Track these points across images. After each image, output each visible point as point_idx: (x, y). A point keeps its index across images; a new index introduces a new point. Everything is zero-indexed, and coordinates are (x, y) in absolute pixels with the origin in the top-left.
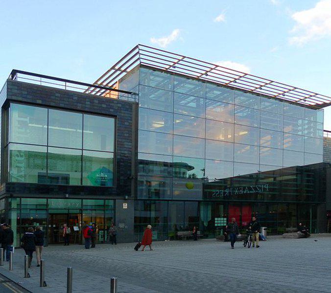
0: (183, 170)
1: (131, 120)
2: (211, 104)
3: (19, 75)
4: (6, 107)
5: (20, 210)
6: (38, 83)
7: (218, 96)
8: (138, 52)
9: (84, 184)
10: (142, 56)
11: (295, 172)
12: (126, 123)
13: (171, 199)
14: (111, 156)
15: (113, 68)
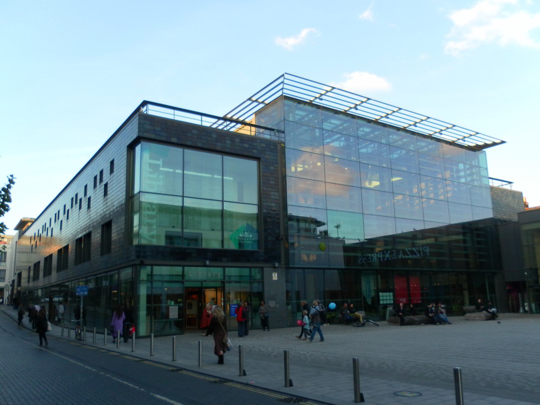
0: (313, 226)
1: (277, 163)
2: (329, 137)
3: (150, 106)
4: (131, 147)
5: (152, 282)
6: (171, 117)
7: (367, 134)
8: (282, 82)
9: (226, 247)
10: (285, 86)
11: (461, 230)
12: (272, 168)
13: (328, 267)
14: (254, 210)
15: (250, 99)
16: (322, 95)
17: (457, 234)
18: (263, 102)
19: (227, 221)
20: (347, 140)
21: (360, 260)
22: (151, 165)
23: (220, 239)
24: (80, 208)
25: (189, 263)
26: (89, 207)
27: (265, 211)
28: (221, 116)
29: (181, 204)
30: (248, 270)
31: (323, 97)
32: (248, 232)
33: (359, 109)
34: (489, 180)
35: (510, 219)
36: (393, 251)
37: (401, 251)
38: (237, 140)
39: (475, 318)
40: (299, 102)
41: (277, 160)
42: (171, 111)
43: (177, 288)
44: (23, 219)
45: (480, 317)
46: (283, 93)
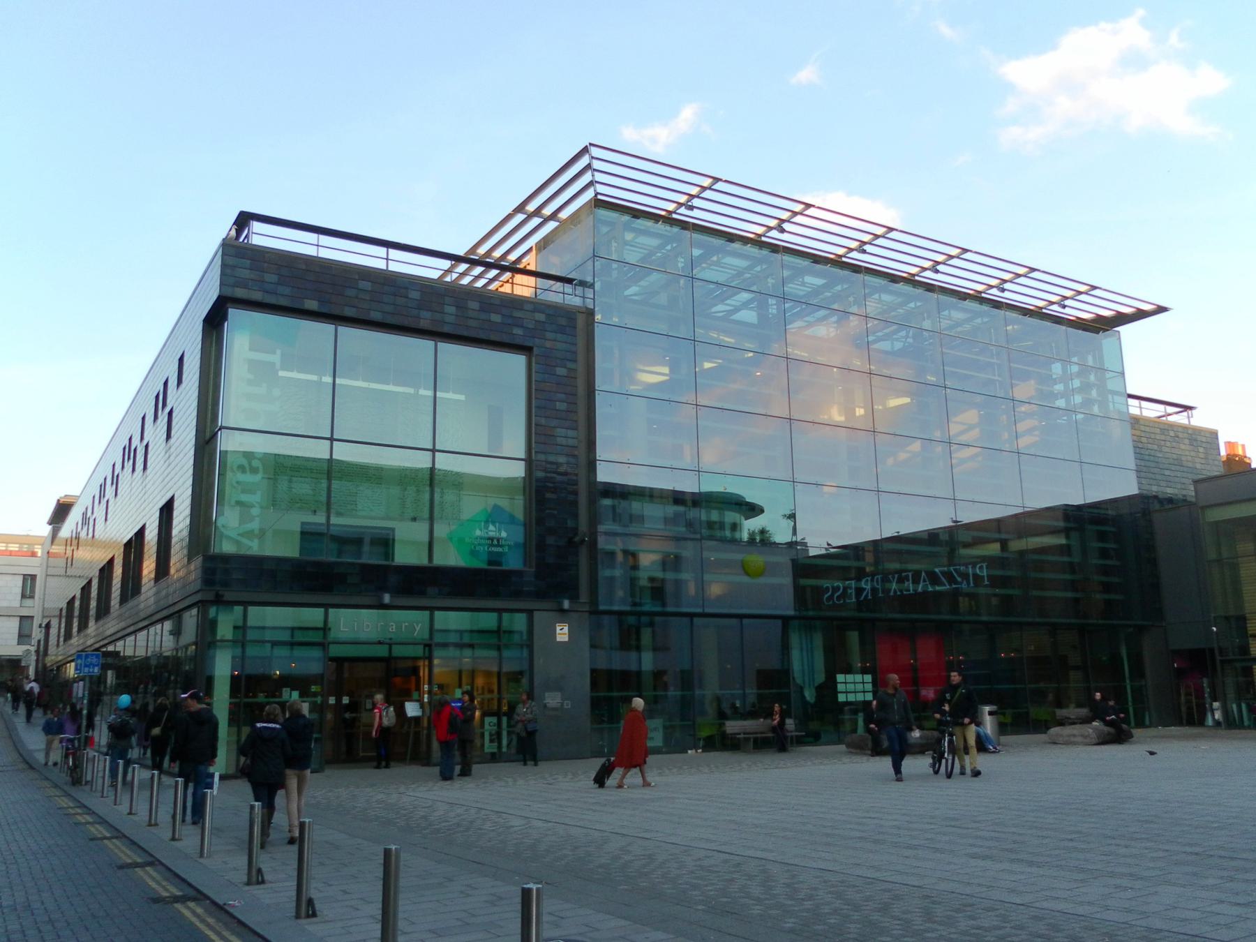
3: (257, 226)
6: (311, 251)
7: (817, 291)
8: (589, 167)
10: (599, 177)
11: (1061, 524)
12: (561, 371)
13: (699, 610)
14: (517, 470)
15: (520, 208)
16: (692, 197)
17: (1054, 532)
18: (553, 216)
19: (446, 497)
20: (762, 308)
21: (826, 596)
22: (253, 365)
23: (426, 539)
24: (134, 470)
25: (337, 600)
26: (145, 468)
27: (540, 474)
28: (461, 253)
29: (327, 457)
30: (494, 615)
31: (696, 202)
32: (497, 525)
33: (787, 229)
34: (1127, 402)
35: (1184, 496)
36: (903, 574)
37: (923, 574)
38: (474, 305)
39: (1072, 739)
40: (731, 238)
41: (575, 353)
42: (311, 237)
43: (310, 663)
44: (62, 500)
45: (1085, 737)
46: (597, 194)
